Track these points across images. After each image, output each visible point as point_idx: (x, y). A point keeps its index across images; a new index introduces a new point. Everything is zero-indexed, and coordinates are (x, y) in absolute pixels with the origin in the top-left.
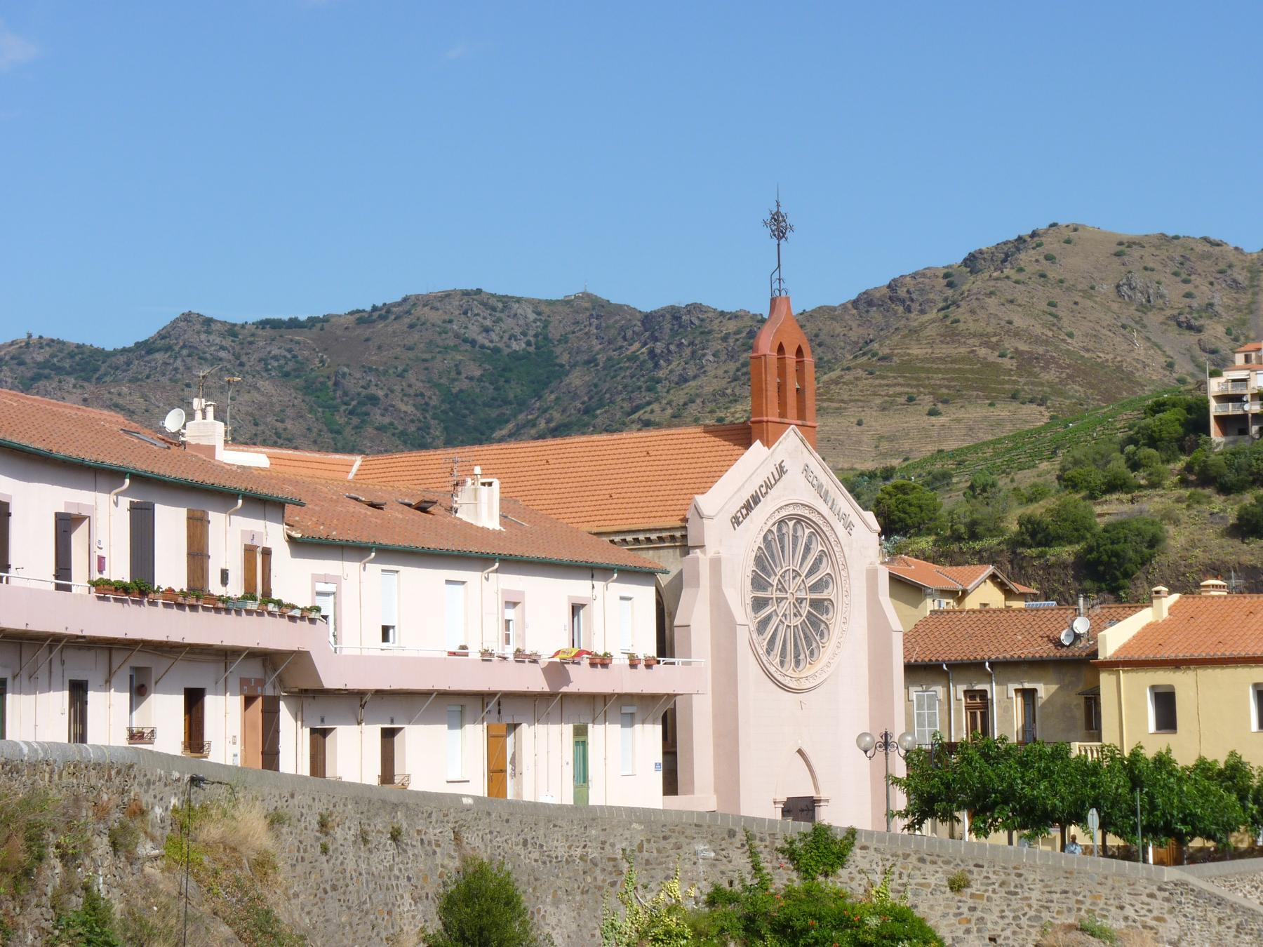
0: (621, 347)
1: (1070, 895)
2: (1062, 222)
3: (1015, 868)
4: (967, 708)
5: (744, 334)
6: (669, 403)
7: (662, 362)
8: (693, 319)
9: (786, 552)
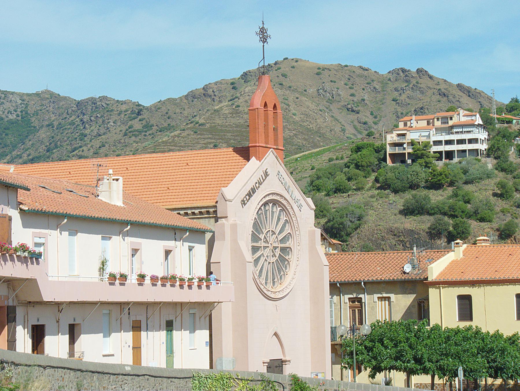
0: (66, 118)
2: (290, 58)
4: (350, 308)
5: (129, 112)
6: (92, 146)
7: (87, 125)
8: (103, 104)
9: (268, 219)
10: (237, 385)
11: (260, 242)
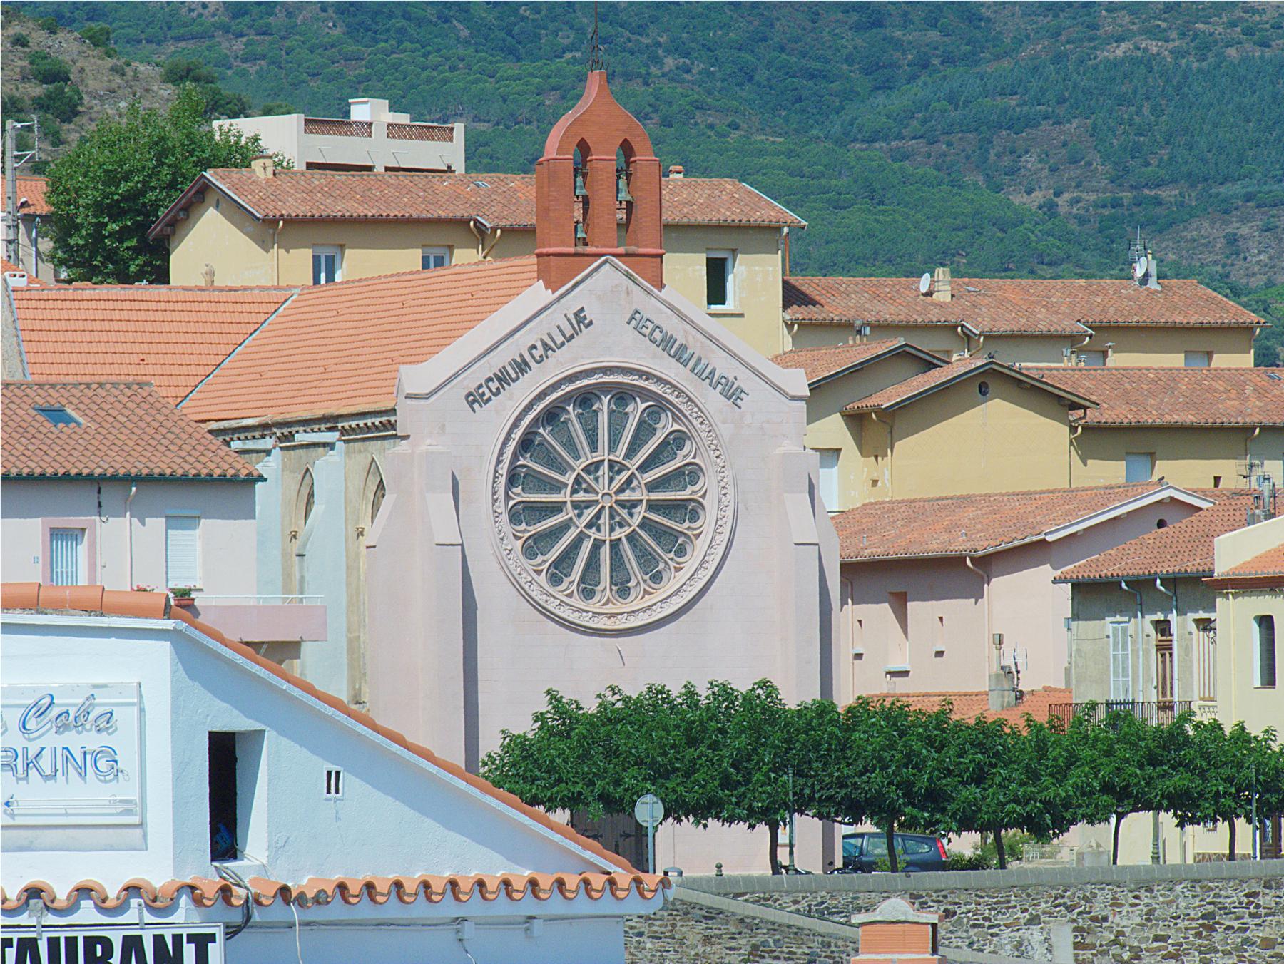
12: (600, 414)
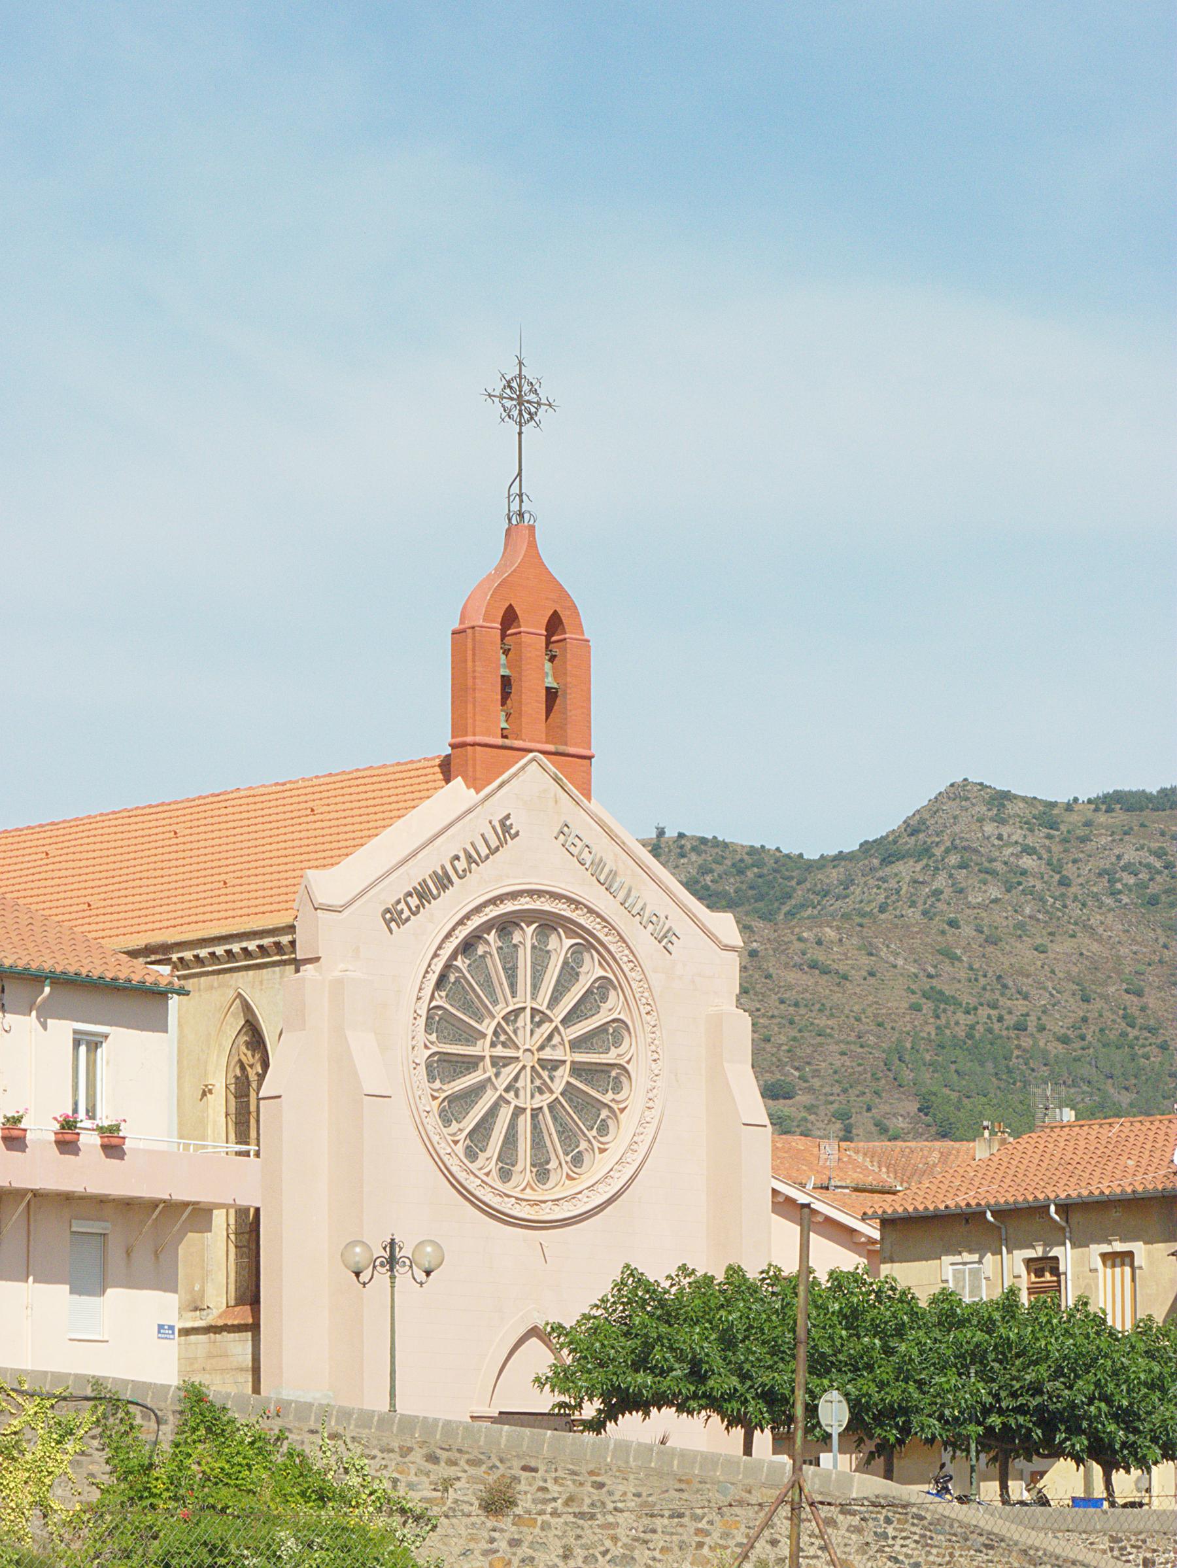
1: (685, 1520)
3: (591, 1473)
10: (18, 1409)
11: (480, 1043)
12: (521, 951)
